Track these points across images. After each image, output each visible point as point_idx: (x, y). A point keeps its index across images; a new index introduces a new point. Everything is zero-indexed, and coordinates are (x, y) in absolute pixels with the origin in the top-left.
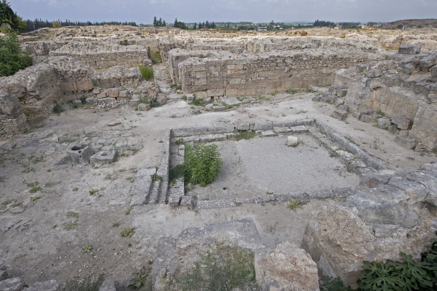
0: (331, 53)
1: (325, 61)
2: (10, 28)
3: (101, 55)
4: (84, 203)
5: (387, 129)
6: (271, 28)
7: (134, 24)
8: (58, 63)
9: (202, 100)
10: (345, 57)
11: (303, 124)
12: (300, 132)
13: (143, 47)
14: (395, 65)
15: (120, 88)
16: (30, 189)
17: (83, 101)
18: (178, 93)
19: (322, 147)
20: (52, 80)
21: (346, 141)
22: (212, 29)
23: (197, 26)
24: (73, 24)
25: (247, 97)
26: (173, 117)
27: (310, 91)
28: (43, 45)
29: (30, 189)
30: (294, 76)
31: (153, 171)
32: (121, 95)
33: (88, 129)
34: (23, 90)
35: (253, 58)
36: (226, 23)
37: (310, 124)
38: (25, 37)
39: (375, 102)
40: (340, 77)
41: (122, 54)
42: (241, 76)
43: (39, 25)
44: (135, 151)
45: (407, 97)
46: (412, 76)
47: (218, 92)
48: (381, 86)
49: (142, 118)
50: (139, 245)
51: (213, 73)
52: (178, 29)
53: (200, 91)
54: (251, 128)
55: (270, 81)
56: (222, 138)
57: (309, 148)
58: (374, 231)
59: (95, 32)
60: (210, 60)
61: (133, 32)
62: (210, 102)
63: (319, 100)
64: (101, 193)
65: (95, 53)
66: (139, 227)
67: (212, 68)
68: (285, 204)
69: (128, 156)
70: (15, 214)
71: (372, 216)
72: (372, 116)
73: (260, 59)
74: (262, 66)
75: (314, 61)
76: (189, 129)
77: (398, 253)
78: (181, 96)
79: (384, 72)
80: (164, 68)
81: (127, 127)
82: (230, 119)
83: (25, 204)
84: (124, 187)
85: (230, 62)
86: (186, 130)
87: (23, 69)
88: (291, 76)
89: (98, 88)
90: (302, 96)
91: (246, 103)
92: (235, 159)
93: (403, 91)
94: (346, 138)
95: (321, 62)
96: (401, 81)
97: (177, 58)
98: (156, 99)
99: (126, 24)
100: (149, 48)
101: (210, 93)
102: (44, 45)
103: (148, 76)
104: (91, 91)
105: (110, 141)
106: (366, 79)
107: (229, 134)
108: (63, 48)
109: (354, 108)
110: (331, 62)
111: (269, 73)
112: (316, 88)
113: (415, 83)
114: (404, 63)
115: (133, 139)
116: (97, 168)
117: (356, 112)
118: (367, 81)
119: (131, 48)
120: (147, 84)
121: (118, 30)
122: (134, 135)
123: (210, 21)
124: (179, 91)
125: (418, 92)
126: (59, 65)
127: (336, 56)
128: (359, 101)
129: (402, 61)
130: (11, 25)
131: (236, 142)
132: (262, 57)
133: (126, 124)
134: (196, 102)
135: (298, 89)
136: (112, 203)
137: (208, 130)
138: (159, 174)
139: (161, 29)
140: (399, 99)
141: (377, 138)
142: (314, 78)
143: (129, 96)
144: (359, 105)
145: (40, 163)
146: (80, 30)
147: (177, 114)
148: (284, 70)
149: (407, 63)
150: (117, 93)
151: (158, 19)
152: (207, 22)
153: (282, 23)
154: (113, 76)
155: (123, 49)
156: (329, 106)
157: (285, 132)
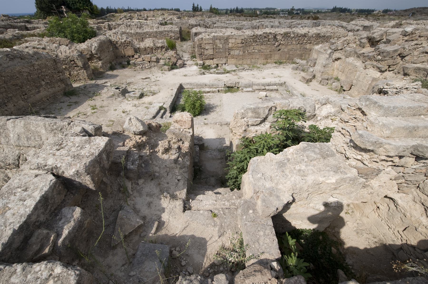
2: (89, 14)
5: (337, 91)
7: (178, 10)
8: (112, 35)
9: (209, 66)
10: (327, 35)
11: (275, 84)
12: (272, 90)
13: (176, 27)
14: (355, 40)
17: (129, 64)
18: (194, 61)
23: (229, 12)
26: (185, 76)
28: (108, 26)
30: (282, 50)
31: (161, 105)
32: (152, 60)
33: (129, 81)
34: (90, 53)
35: (250, 34)
37: (281, 85)
38: (99, 21)
41: (161, 32)
42: (240, 49)
43: (109, 11)
44: (154, 94)
45: (356, 65)
47: (222, 61)
48: (341, 57)
51: (218, 45)
52: (211, 13)
53: (208, 59)
55: (262, 53)
56: (215, 91)
59: (147, 17)
60: (216, 35)
61: (175, 16)
62: (215, 68)
63: (297, 70)
64: (128, 112)
65: (142, 31)
67: (218, 41)
69: (149, 96)
73: (255, 34)
74: (256, 41)
75: (300, 38)
76: (194, 84)
79: (345, 46)
81: (153, 80)
83: (88, 114)
84: (142, 111)
85: (231, 37)
86: (191, 84)
87: (90, 39)
88: (279, 50)
92: (218, 103)
93: (355, 61)
95: (306, 39)
98: (176, 63)
99: (172, 10)
100: (181, 27)
101: (215, 61)
102: (109, 25)
104: (133, 56)
105: (141, 87)
107: (221, 89)
108: (120, 27)
109: (318, 75)
110: (314, 39)
111: (262, 47)
112: (298, 61)
113: (364, 54)
114: (362, 38)
115: (155, 87)
116: (129, 101)
118: (330, 53)
119: (167, 28)
120: (171, 53)
121: (164, 15)
122: (156, 85)
123: (240, 7)
126: (113, 37)
127: (319, 34)
128: (322, 70)
129: (361, 37)
130: (89, 11)
131: (224, 94)
132: (257, 33)
133: (153, 79)
135: (285, 61)
137: (206, 85)
138: (164, 106)
139: (198, 13)
142: (299, 52)
143: (158, 60)
144: (322, 72)
145: (98, 96)
146: (136, 15)
148: (275, 44)
149: (364, 38)
150: (150, 58)
151: (196, 5)
152: (237, 8)
153: (303, 9)
154: (147, 45)
155: (162, 28)
157: (260, 90)
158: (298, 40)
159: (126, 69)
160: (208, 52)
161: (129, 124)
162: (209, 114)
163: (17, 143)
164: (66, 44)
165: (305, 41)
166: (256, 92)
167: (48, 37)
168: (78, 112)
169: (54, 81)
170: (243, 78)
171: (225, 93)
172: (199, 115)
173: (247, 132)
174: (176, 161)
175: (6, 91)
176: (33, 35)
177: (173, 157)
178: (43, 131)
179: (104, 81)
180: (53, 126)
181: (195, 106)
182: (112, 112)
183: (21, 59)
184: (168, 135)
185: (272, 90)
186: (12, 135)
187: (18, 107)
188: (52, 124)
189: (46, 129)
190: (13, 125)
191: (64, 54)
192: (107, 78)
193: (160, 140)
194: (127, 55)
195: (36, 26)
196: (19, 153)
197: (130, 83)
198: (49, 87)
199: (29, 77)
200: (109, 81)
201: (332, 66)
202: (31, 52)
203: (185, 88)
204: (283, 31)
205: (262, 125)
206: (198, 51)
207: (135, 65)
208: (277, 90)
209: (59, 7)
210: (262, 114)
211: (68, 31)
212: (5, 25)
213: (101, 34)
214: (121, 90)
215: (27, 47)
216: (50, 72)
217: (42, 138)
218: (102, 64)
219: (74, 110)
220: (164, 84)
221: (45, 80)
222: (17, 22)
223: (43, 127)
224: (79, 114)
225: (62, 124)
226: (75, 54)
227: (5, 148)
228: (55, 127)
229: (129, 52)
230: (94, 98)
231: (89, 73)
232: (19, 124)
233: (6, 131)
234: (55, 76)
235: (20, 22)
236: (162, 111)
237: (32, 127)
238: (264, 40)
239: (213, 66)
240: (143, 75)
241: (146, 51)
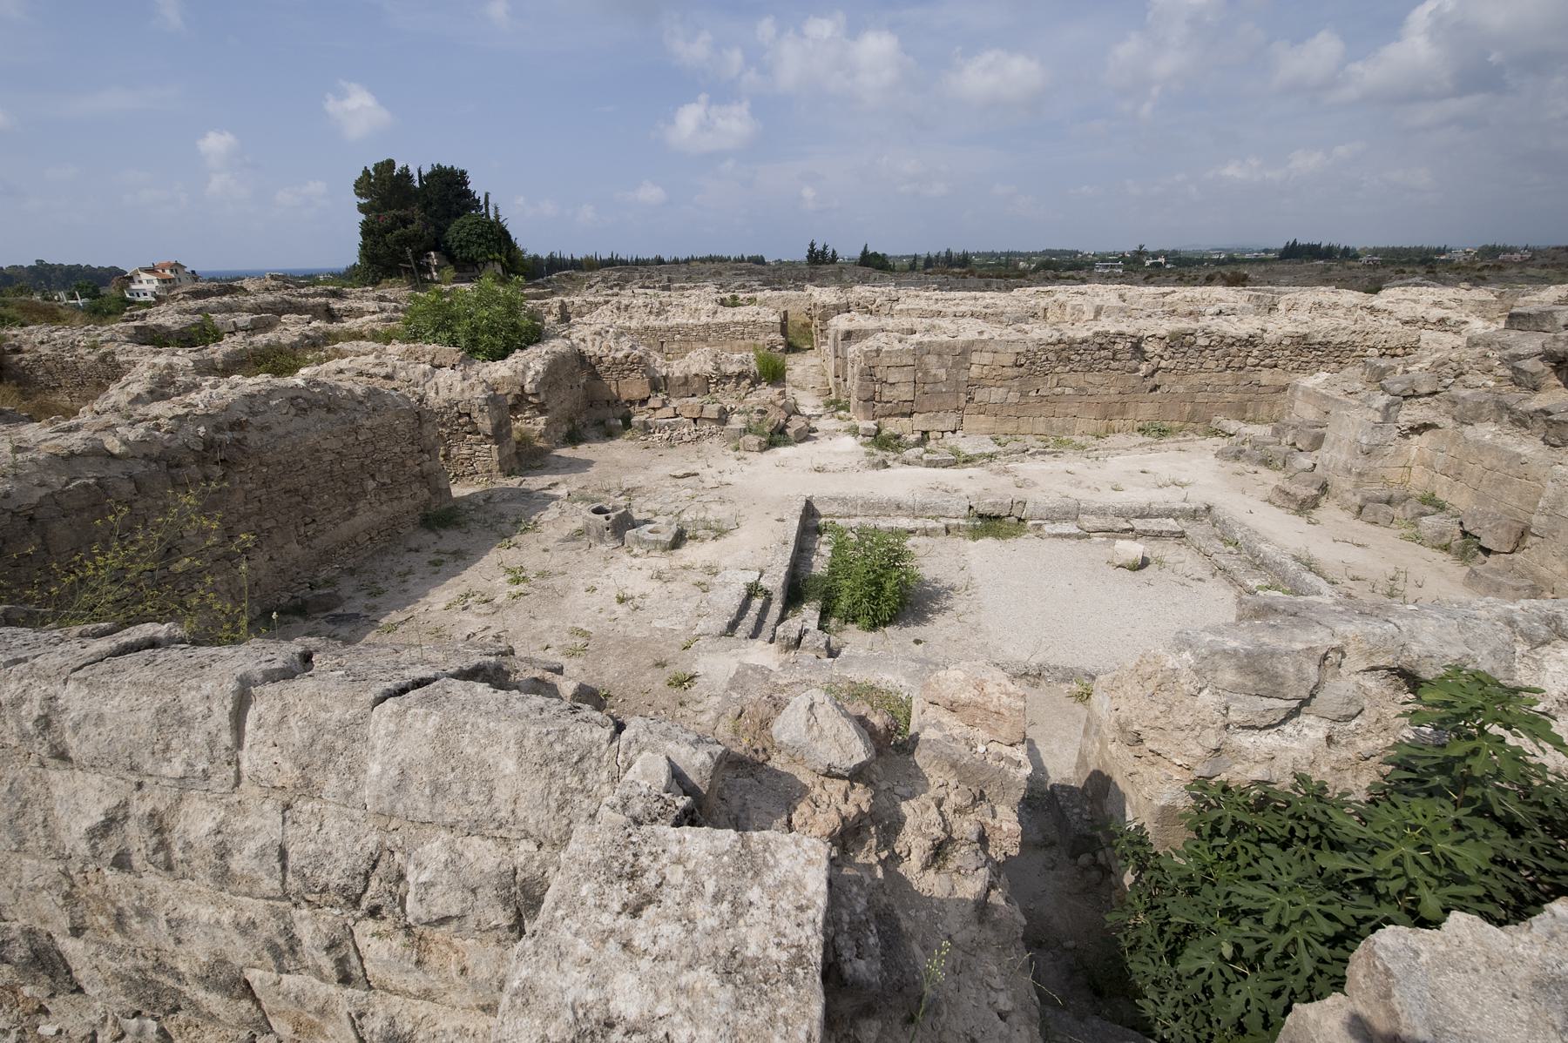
0: (1290, 329)
1: (1269, 351)
3: (676, 329)
4: (603, 615)
5: (1446, 548)
6: (1137, 267)
8: (588, 339)
9: (898, 437)
10: (1337, 340)
11: (1169, 514)
12: (1158, 535)
14: (1487, 364)
15: (707, 398)
16: (509, 577)
17: (627, 424)
19: (1218, 577)
20: (572, 374)
21: (1293, 567)
22: (957, 270)
23: (921, 263)
24: (624, 263)
25: (1020, 437)
27: (1216, 433)
29: (509, 577)
31: (752, 577)
32: (706, 414)
33: (629, 481)
34: (517, 391)
36: (1003, 254)
37: (1194, 515)
39: (1416, 470)
40: (1309, 394)
41: (723, 327)
42: (1007, 383)
43: (555, 265)
44: (720, 533)
45: (1519, 455)
46: (1539, 396)
47: (942, 420)
48: (1437, 421)
49: (745, 468)
50: (700, 707)
51: (933, 372)
54: (1016, 512)
56: (933, 530)
57: (1177, 578)
58: (1227, 708)
59: (669, 280)
60: (926, 339)
63: (1237, 458)
64: (637, 601)
66: (706, 675)
67: (931, 360)
68: (1065, 687)
69: (703, 540)
70: (479, 615)
71: (1229, 676)
72: (1404, 509)
73: (1065, 338)
75: (1234, 350)
77: (1289, 770)
78: (844, 425)
79: (1448, 381)
80: (817, 361)
82: (962, 485)
83: (497, 601)
84: (686, 599)
86: (844, 501)
87: (522, 348)
89: (661, 396)
90: (1183, 445)
91: (1016, 452)
92: (958, 579)
93: (1508, 439)
94: (1296, 559)
95: (1255, 353)
96: (1503, 408)
97: (848, 335)
98: (785, 426)
99: (742, 260)
100: (786, 313)
101: (919, 422)
102: (563, 306)
103: (774, 375)
104: (644, 402)
106: (1386, 399)
107: (954, 522)
109: (1343, 484)
110: (1287, 353)
111: (1089, 377)
112: (1233, 426)
113: (1549, 414)
114: (1518, 357)
115: (720, 508)
116: (636, 556)
117: (1348, 496)
118: (1388, 406)
120: (767, 393)
122: (721, 501)
123: (957, 250)
124: (842, 413)
125: (1558, 442)
126: (590, 344)
127: (1305, 337)
128: (1360, 464)
129: (1512, 351)
130: (503, 266)
131: (970, 543)
132: (1071, 334)
133: (709, 476)
134: (882, 441)
135: (1177, 424)
136: (657, 624)
137: (899, 507)
140: (1495, 462)
141: (1403, 568)
142: (1230, 397)
143: (723, 417)
144: (1360, 474)
145: (529, 534)
147: (832, 468)
148: (1137, 370)
149: (1528, 356)
151: (819, 247)
152: (948, 252)
153: (1175, 252)
156: (1264, 473)
158: (1224, 357)
159: (618, 442)
160: (895, 393)
161: (810, 728)
162: (928, 620)
163: (386, 805)
164: (450, 363)
165: (1250, 361)
166: (1097, 538)
167: (402, 341)
168: (463, 589)
169: (401, 479)
170: (1035, 484)
171: (974, 539)
172: (892, 620)
173: (1225, 757)
174: (982, 907)
175: (260, 512)
176: (358, 336)
177: (971, 888)
178: (509, 765)
179: (546, 480)
180: (551, 744)
181: (880, 588)
182: (581, 597)
183: (329, 411)
184: (926, 771)
185: (1158, 535)
186: (375, 769)
187: (278, 564)
188: (551, 738)
189: (521, 758)
190: (392, 727)
191: (444, 394)
192: (556, 471)
193: (905, 799)
194: (624, 397)
195: (356, 305)
196: (380, 844)
197: (633, 490)
198: (384, 497)
199: (336, 467)
200: (565, 482)
201: (1398, 453)
202: (359, 390)
203: (822, 513)
204: (1166, 326)
205: (1288, 728)
206: (860, 388)
207: (646, 428)
208: (1182, 535)
209: (420, 254)
210: (1292, 681)
211: (462, 328)
212: (274, 303)
213: (557, 336)
214: (612, 515)
215: (341, 371)
216: (397, 449)
217: (497, 793)
218: (547, 424)
219: (450, 581)
220: (752, 502)
221: (378, 476)
222: (307, 296)
223: (513, 748)
224: (467, 596)
225: (587, 735)
226: (479, 394)
227: (327, 814)
228: (558, 748)
229: (634, 387)
230: (517, 538)
231: (506, 451)
232: (418, 725)
233: (357, 745)
234: (410, 463)
235: (315, 295)
236: (757, 603)
237: (467, 741)
238: (1096, 355)
239: (913, 438)
240: (674, 462)
241: (686, 385)
